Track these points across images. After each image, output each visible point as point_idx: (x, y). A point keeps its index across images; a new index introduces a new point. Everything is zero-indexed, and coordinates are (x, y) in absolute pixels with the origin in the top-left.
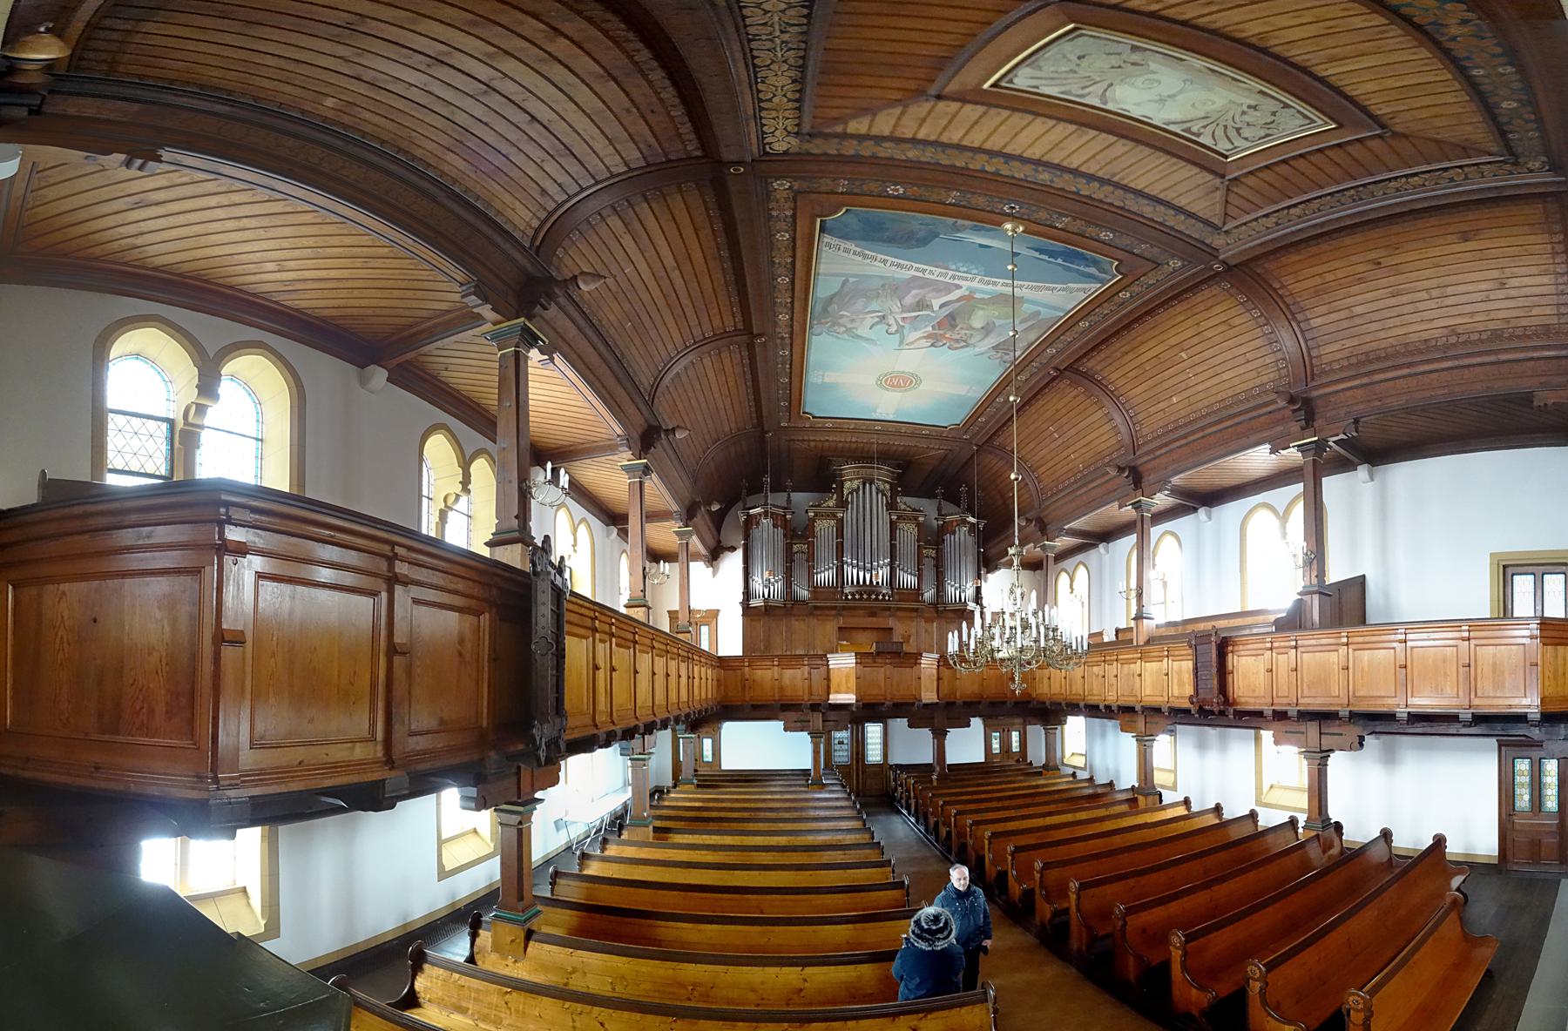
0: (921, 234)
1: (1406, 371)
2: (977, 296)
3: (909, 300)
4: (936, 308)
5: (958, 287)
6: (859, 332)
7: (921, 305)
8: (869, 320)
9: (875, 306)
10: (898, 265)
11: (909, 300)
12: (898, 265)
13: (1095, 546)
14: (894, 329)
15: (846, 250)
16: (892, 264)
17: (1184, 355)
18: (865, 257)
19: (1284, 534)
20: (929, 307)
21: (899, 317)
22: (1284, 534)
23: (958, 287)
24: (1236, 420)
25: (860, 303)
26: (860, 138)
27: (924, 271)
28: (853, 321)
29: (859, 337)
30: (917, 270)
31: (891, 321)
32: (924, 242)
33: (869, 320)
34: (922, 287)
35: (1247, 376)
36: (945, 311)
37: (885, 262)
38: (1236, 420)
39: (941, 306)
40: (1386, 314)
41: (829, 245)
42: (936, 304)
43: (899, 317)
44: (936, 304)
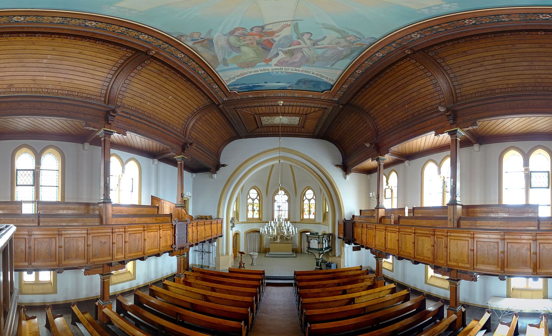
0: (301, 84)
1: (156, 127)
2: (264, 63)
3: (299, 55)
4: (280, 52)
5: (276, 65)
6: (335, 35)
7: (291, 53)
8: (325, 42)
9: (320, 52)
10: (307, 72)
11: (299, 55)
12: (307, 72)
13: (402, 162)
14: (306, 37)
15: (327, 78)
16: (310, 72)
17: (171, 97)
18: (321, 76)
19: (439, 173)
20: (285, 53)
21: (303, 45)
22: (439, 173)
23: (276, 65)
24: (169, 133)
25: (329, 53)
26: (317, 107)
27: (296, 70)
28: (338, 43)
29: (338, 31)
30: (299, 70)
31: (308, 42)
32: (299, 81)
33: (325, 42)
34: (294, 63)
35: (175, 121)
36: (273, 51)
37: (313, 73)
38: (169, 133)
39: (277, 55)
40: (80, 74)
41: (333, 80)
42: (282, 56)
43: (303, 45)
44: (282, 56)
